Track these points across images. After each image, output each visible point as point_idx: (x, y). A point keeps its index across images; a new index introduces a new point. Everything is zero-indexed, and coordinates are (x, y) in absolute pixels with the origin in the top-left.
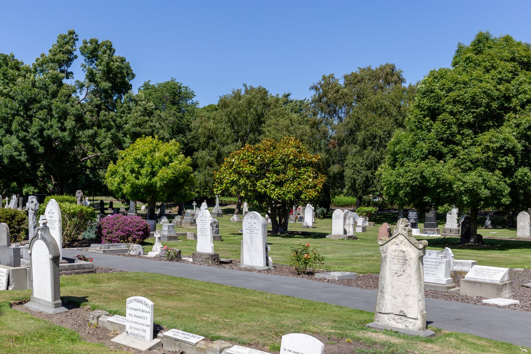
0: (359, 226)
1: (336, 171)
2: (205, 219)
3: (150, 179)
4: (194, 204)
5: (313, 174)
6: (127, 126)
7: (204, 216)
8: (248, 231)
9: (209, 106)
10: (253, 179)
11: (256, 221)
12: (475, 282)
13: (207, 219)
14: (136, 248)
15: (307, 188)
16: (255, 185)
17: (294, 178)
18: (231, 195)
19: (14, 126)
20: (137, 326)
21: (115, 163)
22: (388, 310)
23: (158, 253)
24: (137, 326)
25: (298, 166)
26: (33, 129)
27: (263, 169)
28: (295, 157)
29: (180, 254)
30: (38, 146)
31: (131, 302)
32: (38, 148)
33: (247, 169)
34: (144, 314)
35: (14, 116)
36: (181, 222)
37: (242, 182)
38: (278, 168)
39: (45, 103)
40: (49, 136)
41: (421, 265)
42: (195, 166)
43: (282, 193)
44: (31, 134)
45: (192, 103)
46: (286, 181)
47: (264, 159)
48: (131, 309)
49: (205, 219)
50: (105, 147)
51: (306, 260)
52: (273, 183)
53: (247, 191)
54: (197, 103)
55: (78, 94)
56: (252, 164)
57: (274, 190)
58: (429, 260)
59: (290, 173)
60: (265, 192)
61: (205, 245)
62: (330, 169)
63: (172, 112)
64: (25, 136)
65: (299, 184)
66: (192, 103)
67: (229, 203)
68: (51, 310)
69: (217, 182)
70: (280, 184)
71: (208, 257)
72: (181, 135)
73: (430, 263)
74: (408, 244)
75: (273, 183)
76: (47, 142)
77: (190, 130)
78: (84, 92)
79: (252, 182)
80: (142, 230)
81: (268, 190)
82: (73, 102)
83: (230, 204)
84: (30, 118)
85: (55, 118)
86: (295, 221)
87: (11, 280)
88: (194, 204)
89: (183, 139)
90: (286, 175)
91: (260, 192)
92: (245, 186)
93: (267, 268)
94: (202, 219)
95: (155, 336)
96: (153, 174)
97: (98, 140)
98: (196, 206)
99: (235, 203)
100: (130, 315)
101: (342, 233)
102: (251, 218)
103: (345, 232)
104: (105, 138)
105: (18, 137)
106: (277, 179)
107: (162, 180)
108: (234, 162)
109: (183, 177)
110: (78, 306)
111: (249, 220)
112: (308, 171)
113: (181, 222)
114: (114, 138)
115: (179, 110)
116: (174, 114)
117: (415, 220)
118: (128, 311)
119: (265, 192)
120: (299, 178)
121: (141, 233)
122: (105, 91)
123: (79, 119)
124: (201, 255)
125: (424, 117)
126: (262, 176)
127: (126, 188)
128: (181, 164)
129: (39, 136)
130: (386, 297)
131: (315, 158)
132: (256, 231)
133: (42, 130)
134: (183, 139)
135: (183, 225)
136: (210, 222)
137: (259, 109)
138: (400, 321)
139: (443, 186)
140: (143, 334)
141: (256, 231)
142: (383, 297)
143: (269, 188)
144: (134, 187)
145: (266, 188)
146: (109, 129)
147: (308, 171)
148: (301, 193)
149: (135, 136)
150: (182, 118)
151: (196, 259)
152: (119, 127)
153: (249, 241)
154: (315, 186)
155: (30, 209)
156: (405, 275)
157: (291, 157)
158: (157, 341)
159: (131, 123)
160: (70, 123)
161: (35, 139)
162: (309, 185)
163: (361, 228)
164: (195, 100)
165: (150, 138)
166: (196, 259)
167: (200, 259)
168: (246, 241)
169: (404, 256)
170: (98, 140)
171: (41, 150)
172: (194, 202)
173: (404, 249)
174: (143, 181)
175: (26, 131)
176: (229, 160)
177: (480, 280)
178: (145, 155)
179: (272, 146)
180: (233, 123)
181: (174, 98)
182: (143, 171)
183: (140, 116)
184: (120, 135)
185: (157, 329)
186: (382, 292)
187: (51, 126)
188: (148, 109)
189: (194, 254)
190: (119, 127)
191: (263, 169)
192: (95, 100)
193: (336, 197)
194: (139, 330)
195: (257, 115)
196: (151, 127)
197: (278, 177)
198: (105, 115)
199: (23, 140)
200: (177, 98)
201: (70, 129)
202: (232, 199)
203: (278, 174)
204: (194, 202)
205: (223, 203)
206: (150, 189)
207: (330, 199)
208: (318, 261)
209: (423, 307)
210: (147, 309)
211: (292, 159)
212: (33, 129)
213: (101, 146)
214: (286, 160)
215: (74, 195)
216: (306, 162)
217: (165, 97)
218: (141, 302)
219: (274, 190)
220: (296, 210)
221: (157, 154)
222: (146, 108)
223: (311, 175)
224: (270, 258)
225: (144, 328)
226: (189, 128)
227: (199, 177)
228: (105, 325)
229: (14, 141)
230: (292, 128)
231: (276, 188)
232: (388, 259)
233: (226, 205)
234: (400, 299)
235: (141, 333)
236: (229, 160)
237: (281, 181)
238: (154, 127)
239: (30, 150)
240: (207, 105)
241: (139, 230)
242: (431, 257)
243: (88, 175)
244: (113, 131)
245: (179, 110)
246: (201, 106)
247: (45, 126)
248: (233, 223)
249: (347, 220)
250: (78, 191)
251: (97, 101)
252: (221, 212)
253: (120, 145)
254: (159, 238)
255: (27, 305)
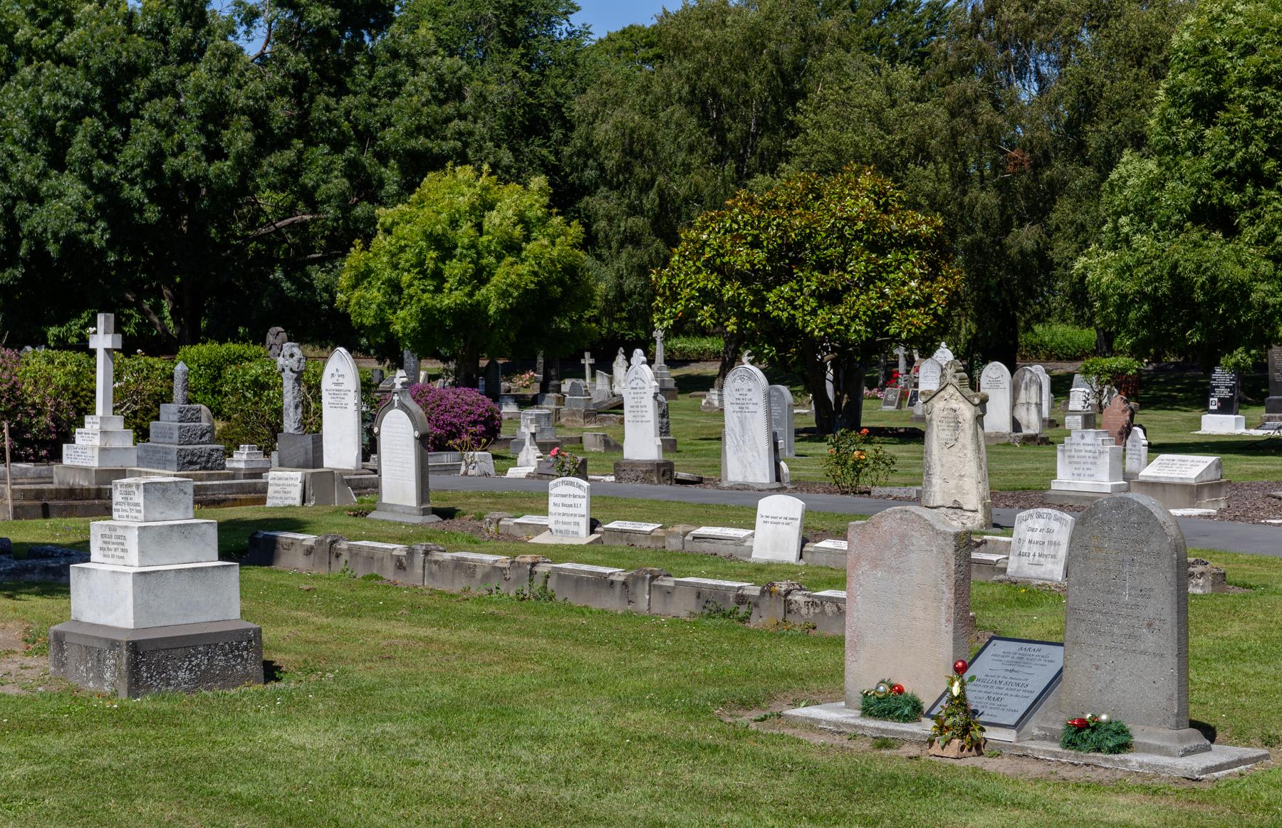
0: (1075, 412)
1: (1029, 245)
2: (641, 384)
3: (471, 295)
4: (588, 361)
5: (922, 267)
6: (389, 135)
7: (637, 381)
8: (736, 408)
9: (623, 32)
10: (758, 285)
11: (751, 385)
12: (1154, 484)
13: (647, 386)
14: (481, 460)
15: (904, 305)
16: (765, 300)
17: (869, 280)
18: (703, 332)
19: (79, 146)
20: (566, 519)
21: (366, 247)
22: (937, 499)
23: (531, 469)
24: (566, 519)
25: (878, 247)
26: (134, 152)
27: (787, 259)
28: (871, 224)
29: (585, 468)
30: (142, 204)
31: (556, 485)
32: (141, 211)
33: (742, 257)
34: (577, 501)
35: (76, 116)
36: (558, 411)
37: (728, 292)
38: (828, 252)
39: (161, 75)
40: (176, 174)
41: (980, 430)
42: (589, 242)
43: (835, 319)
44: (122, 169)
45: (570, 34)
46: (847, 289)
47: (785, 232)
48: (557, 496)
49: (641, 384)
50: (329, 198)
51: (857, 462)
52: (812, 294)
53: (741, 315)
54: (586, 32)
55: (241, 42)
56: (756, 244)
57: (814, 312)
58: (1081, 447)
59: (858, 267)
60: (792, 318)
61: (641, 442)
62: (1008, 240)
63: (509, 67)
64: (109, 174)
65: (883, 296)
66: (570, 34)
67: (695, 356)
68: (419, 519)
69: (661, 296)
70: (832, 297)
71: (649, 468)
72: (538, 141)
73: (1083, 454)
74: (961, 398)
75: (812, 294)
76: (169, 190)
77: (569, 126)
78: (260, 31)
79: (756, 293)
80: (481, 423)
81: (798, 314)
82: (242, 75)
83: (697, 361)
84: (123, 120)
85: (190, 121)
86: (899, 406)
87: (310, 492)
88: (588, 361)
89: (545, 152)
90: (845, 271)
91: (778, 320)
92: (736, 303)
93: (777, 485)
94: (634, 384)
95: (592, 531)
96: (480, 276)
97: (308, 179)
98: (594, 368)
99: (716, 356)
100: (555, 504)
101: (1006, 427)
102: (742, 378)
103: (1016, 425)
104: (328, 174)
105: (86, 178)
106: (822, 284)
107: (504, 295)
108: (705, 242)
109: (560, 282)
110: (452, 517)
111: (738, 384)
112: (907, 260)
113: (558, 411)
114: (353, 170)
115: (530, 61)
116: (515, 74)
117: (1231, 389)
118: (551, 508)
119: (792, 318)
120: (882, 279)
121: (479, 429)
122: (323, 32)
123: (259, 118)
124: (634, 465)
125: (1184, 117)
126: (783, 275)
127: (403, 320)
128: (556, 242)
129: (146, 175)
130: (934, 481)
131: (927, 223)
132: (751, 408)
133: (157, 157)
134: (545, 152)
135: (563, 420)
136: (653, 391)
137: (786, 52)
138: (954, 517)
139: (1226, 296)
140: (575, 528)
141: (751, 408)
142: (930, 482)
143: (802, 306)
144: (428, 315)
145: (795, 308)
146: (338, 146)
147: (907, 260)
148: (888, 317)
149: (418, 166)
150: (537, 84)
151: (622, 475)
152: (365, 136)
153: (738, 429)
154: (928, 299)
155: (287, 370)
156: (959, 445)
157: (860, 225)
158: (595, 536)
159: (403, 123)
160: (239, 138)
161: (133, 182)
162: (909, 298)
163: (1079, 418)
164: (576, 20)
165: (465, 172)
166: (622, 475)
167: (633, 475)
168: (732, 430)
169: (956, 417)
170: (308, 179)
171: (152, 214)
172: (587, 355)
173: (955, 406)
174: (452, 298)
175: (109, 159)
176: (693, 234)
177: (1163, 480)
178: (454, 223)
179: (811, 191)
180: (703, 103)
181: (511, 24)
182: (454, 269)
183: (428, 103)
184: (367, 159)
185: (593, 525)
186: (928, 474)
187: (181, 148)
188: (448, 77)
189: (617, 465)
190: (365, 136)
191: (787, 259)
192: (293, 58)
193: (1038, 328)
194: (569, 523)
195: (782, 74)
196: (460, 134)
197: (825, 278)
198: (328, 109)
199: (104, 186)
200: (521, 22)
201: (239, 156)
202: (707, 344)
203: (825, 272)
204: (587, 355)
205: (677, 356)
206: (468, 320)
207: (1014, 336)
208: (883, 465)
209: (987, 493)
210: (581, 493)
211: (861, 230)
212: (134, 152)
213: (318, 196)
214: (847, 231)
215: (264, 343)
216: (902, 236)
217: (484, 20)
218: (572, 484)
219: (814, 312)
220: (908, 372)
221: (493, 218)
222: (442, 75)
223: (916, 270)
224: (783, 464)
225: (577, 519)
226: (562, 117)
227: (602, 281)
228: (511, 531)
229: (73, 189)
230: (891, 114)
231: (821, 307)
232: (935, 423)
233: (686, 362)
234: (952, 483)
235: (572, 528)
236: (693, 234)
237: (834, 290)
238: (471, 134)
239: (114, 209)
240: (616, 28)
241: (474, 423)
242: (1085, 441)
243: (276, 283)
244: (351, 152)
245: (530, 61)
246: (599, 33)
247: (167, 145)
248: (707, 415)
249: (1023, 392)
250: (274, 330)
251: (297, 61)
252: (672, 385)
253: (367, 188)
254: (533, 435)
255: (373, 515)
